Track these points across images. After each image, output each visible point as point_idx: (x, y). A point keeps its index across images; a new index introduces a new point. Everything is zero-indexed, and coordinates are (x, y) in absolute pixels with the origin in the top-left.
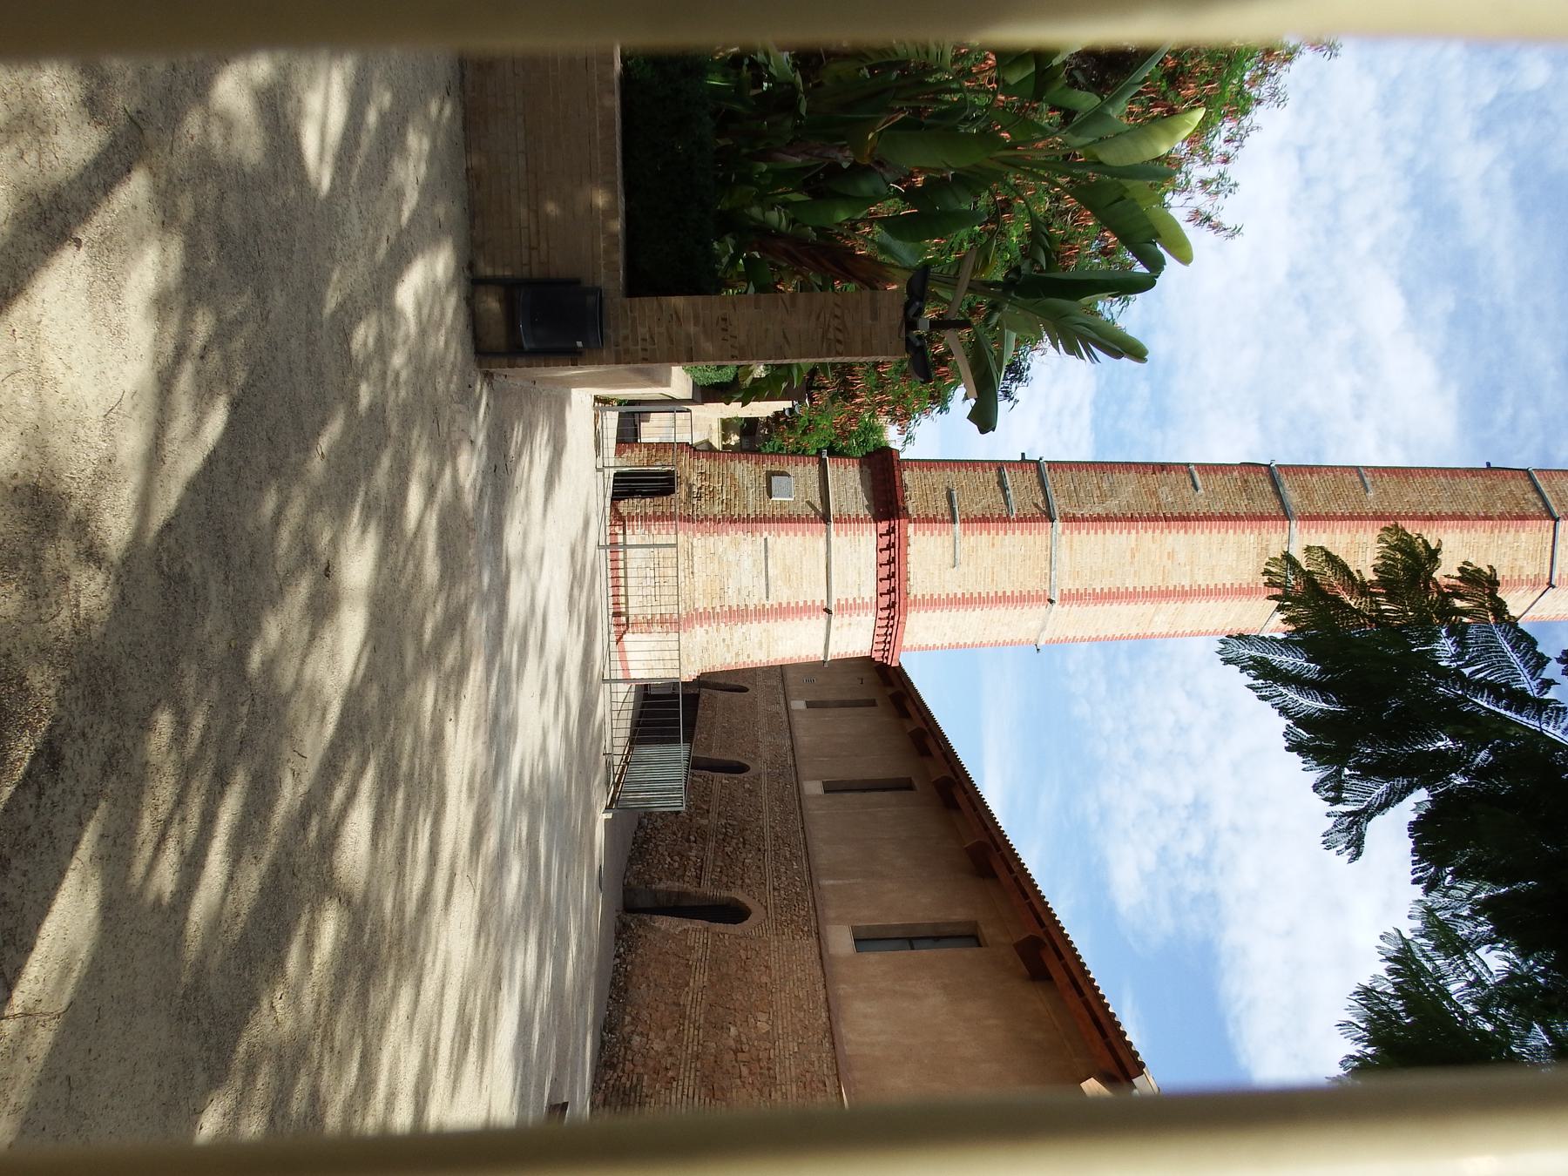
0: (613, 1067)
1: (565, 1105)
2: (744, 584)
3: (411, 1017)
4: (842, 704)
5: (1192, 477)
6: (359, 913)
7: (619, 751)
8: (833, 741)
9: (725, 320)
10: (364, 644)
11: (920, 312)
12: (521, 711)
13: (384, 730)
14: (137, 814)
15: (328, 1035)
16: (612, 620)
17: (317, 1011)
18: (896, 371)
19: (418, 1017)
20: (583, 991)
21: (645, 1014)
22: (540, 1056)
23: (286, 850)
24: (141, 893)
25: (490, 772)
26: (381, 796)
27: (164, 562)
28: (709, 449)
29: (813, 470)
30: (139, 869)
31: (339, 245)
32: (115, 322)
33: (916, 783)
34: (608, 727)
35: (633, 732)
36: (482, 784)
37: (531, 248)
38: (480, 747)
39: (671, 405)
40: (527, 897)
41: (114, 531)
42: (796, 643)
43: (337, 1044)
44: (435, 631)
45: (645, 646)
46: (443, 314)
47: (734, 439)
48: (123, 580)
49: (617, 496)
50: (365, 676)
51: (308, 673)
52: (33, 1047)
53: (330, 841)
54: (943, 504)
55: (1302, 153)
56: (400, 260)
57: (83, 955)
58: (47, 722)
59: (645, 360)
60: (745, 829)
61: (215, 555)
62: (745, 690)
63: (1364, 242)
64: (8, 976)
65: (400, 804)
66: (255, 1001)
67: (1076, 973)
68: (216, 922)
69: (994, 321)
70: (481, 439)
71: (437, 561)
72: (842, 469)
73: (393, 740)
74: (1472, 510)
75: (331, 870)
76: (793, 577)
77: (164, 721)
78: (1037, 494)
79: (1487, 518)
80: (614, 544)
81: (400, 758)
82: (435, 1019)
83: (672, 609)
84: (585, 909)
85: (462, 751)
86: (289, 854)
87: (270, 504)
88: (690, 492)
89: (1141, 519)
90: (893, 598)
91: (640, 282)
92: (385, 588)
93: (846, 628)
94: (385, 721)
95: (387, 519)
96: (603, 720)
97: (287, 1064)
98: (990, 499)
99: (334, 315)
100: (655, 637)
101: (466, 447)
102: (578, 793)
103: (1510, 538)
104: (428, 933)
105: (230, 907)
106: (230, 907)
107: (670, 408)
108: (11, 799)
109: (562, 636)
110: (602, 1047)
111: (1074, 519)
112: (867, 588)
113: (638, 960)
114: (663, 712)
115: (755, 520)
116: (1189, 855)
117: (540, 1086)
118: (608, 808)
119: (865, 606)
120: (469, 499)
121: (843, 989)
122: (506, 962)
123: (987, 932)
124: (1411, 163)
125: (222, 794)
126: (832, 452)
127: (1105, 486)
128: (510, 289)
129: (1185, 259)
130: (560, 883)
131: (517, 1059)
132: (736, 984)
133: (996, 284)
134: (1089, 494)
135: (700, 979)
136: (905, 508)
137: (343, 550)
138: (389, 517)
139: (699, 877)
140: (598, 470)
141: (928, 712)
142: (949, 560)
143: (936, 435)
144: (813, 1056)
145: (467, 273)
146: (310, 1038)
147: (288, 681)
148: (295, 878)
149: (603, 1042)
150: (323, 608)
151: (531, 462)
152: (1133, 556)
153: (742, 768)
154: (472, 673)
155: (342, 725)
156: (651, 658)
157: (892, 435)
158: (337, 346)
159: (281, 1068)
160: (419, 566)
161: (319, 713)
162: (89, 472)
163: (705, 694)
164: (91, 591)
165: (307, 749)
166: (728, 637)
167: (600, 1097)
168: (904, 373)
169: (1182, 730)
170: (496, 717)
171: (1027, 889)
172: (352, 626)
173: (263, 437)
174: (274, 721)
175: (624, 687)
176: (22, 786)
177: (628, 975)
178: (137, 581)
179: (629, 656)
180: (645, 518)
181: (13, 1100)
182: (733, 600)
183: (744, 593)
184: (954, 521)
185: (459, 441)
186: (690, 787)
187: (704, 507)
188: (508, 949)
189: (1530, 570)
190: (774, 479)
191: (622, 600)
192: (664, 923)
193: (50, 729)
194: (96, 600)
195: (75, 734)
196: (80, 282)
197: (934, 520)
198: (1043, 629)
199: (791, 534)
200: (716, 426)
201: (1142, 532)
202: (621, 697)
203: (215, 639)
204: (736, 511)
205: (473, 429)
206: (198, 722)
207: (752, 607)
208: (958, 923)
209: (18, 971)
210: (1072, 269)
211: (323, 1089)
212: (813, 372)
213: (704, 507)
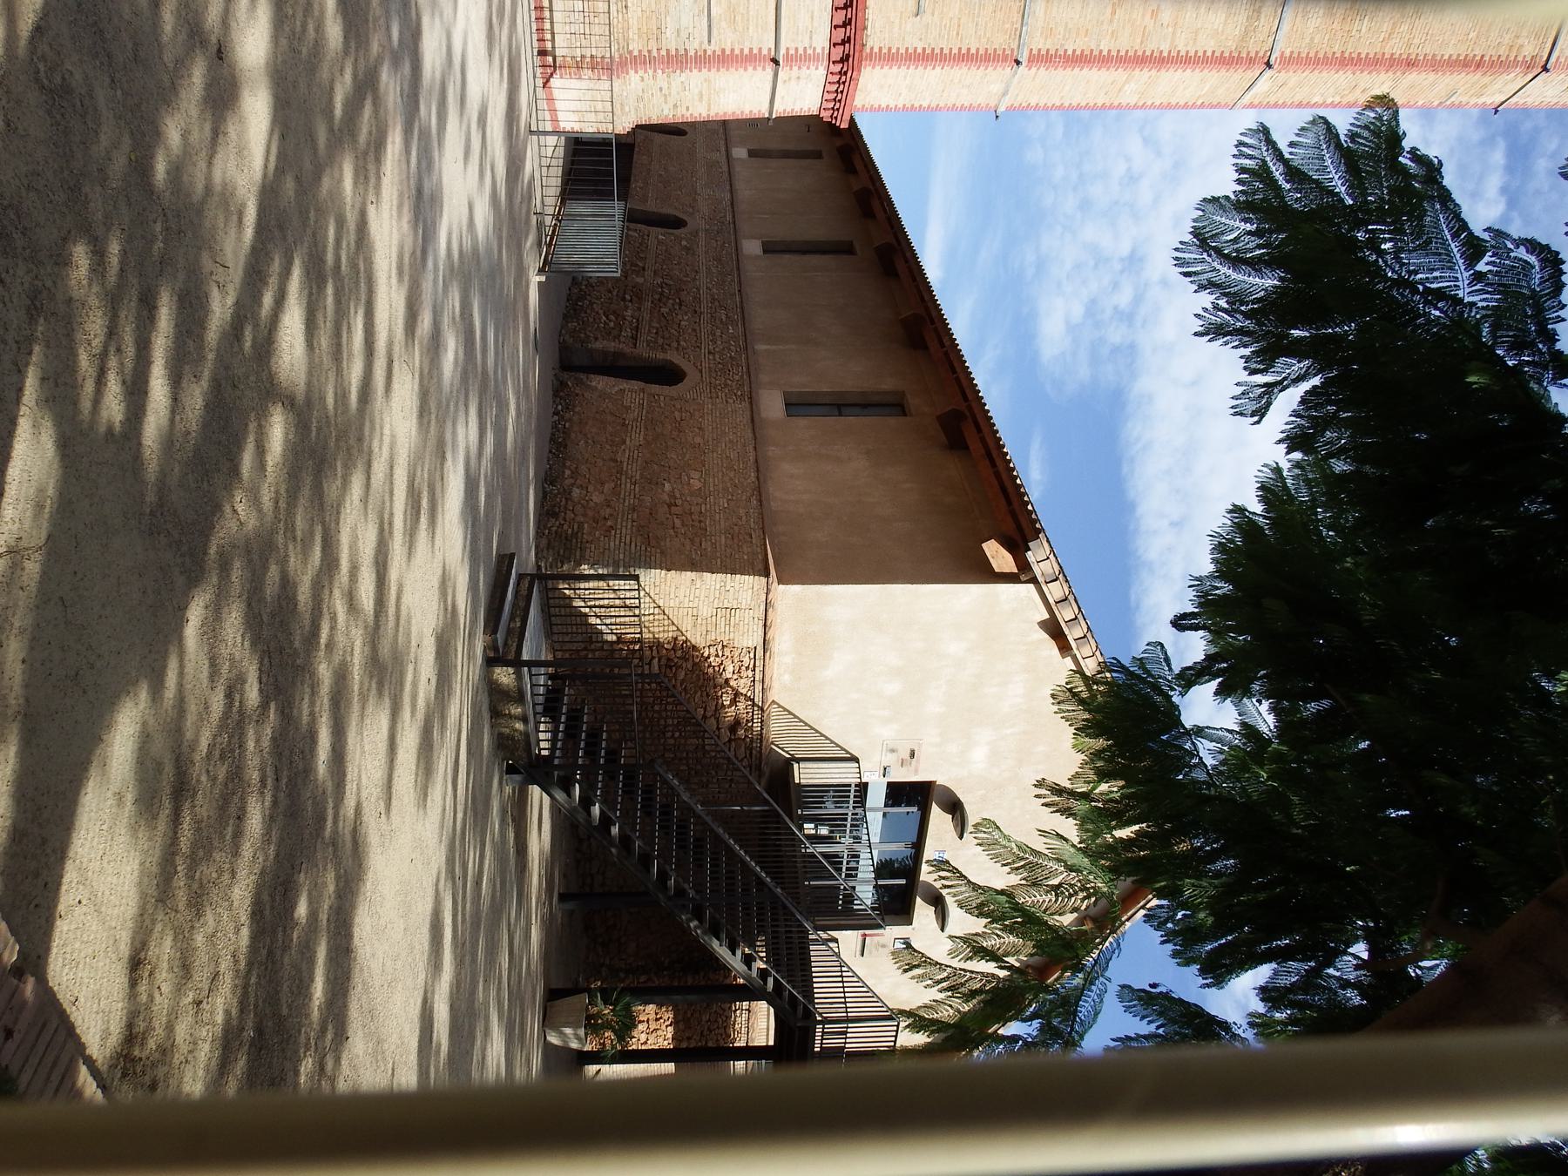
0: (555, 515)
1: (512, 556)
3: (365, 500)
4: (786, 155)
6: (302, 411)
7: (550, 210)
8: (778, 199)
13: (305, 224)
14: (73, 354)
15: (290, 529)
16: (538, 60)
17: (276, 507)
21: (583, 468)
22: (486, 515)
23: (223, 364)
25: (419, 253)
26: (310, 294)
27: (42, 74)
30: (86, 405)
33: (857, 247)
34: (537, 183)
38: (406, 226)
42: (739, 96)
43: (299, 534)
44: (346, 105)
50: (277, 168)
52: (25, 578)
57: (50, 492)
65: (330, 300)
66: (218, 508)
68: (169, 441)
71: (339, 20)
73: (314, 235)
75: (271, 377)
77: (81, 255)
81: (324, 251)
82: (387, 498)
84: (521, 370)
85: (388, 231)
86: (227, 368)
92: (284, 62)
94: (303, 214)
96: (533, 177)
97: (255, 557)
100: (584, 84)
102: (509, 258)
104: (372, 422)
106: (179, 427)
109: (484, 82)
110: (543, 498)
113: (575, 418)
114: (595, 165)
116: (1116, 308)
117: (489, 541)
118: (541, 271)
121: (772, 451)
122: (448, 436)
123: (913, 402)
130: (496, 353)
131: (466, 522)
132: (670, 443)
135: (636, 438)
137: (234, 24)
139: (634, 338)
141: (876, 170)
144: (742, 512)
146: (273, 532)
148: (238, 385)
150: (222, 97)
153: (678, 223)
155: (261, 228)
156: (581, 107)
159: (250, 561)
160: (319, 28)
161: (235, 218)
166: (665, 86)
167: (544, 542)
169: (1132, 179)
170: (419, 191)
172: (256, 111)
174: (190, 234)
175: (552, 140)
177: (566, 432)
178: (19, 102)
179: (559, 105)
181: (17, 624)
182: (671, 43)
183: (684, 35)
186: (625, 241)
188: (449, 424)
189: (1529, 50)
192: (600, 382)
198: (1004, 94)
206: (114, 248)
207: (692, 53)
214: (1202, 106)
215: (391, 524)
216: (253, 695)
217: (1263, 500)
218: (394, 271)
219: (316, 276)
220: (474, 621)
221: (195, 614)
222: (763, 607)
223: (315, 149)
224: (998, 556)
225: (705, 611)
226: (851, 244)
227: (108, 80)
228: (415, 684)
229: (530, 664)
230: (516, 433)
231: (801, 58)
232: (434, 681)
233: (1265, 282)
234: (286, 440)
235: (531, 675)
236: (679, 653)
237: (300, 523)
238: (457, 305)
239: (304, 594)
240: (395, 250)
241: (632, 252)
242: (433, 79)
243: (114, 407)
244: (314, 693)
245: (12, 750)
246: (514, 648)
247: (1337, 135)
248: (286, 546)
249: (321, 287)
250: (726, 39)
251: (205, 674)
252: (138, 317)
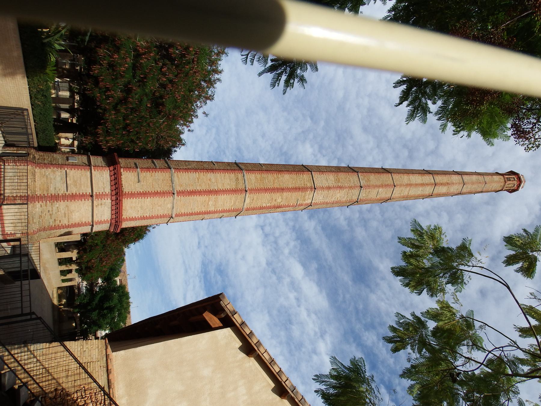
45: (12, 211)
55: (262, 228)
63: (286, 251)
76: (78, 184)
90: (117, 193)
93: (100, 206)
103: (301, 176)
119: (107, 195)
124: (294, 227)
142: (136, 179)
166: (51, 210)
179: (6, 225)
182: (52, 191)
184: (137, 168)
199: (76, 169)
222: (105, 359)
231: (101, 196)
250: (73, 190)
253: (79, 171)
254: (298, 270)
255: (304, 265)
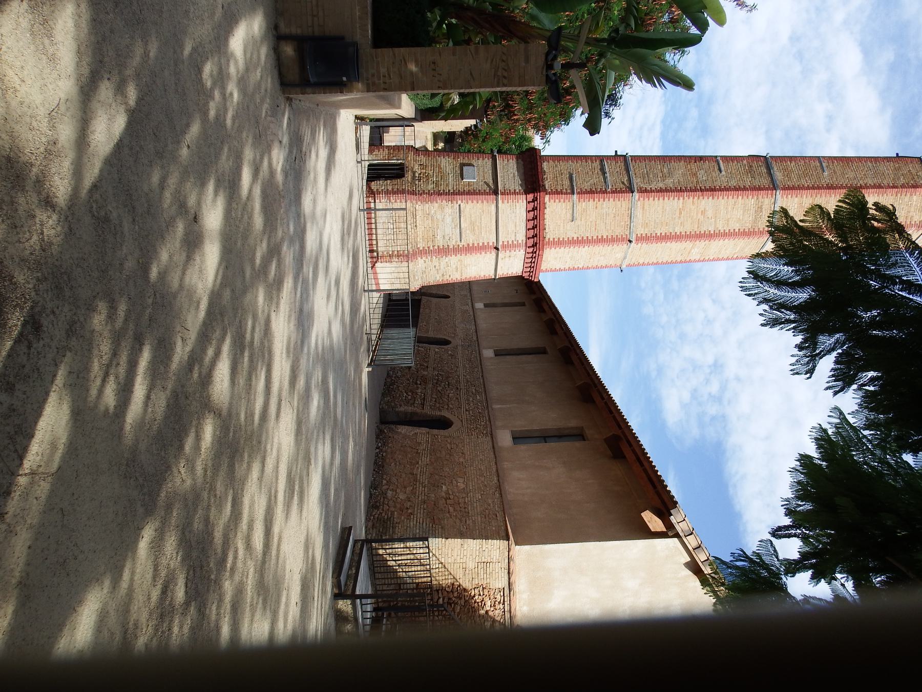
0: (377, 508)
1: (351, 527)
2: (447, 233)
3: (260, 479)
5: (719, 164)
6: (226, 421)
7: (374, 332)
8: (499, 326)
9: (434, 63)
10: (220, 264)
11: (555, 58)
12: (316, 308)
14: (89, 359)
15: (212, 489)
16: (369, 255)
17: (205, 471)
18: (539, 99)
19: (264, 479)
20: (358, 467)
21: (394, 480)
22: (335, 501)
24: (96, 406)
25: (299, 342)
26: (235, 354)
27: (94, 209)
28: (424, 150)
29: (488, 162)
30: (94, 392)
31: (192, 10)
32: (51, 51)
33: (548, 350)
34: (368, 318)
35: (383, 321)
36: (295, 349)
37: (313, 16)
39: (402, 122)
40: (324, 414)
41: (61, 188)
42: (478, 268)
43: (218, 493)
44: (263, 258)
45: (388, 270)
46: (259, 58)
47: (441, 145)
48: (70, 218)
49: (370, 179)
50: (222, 283)
51: (187, 279)
52: (39, 492)
53: (207, 379)
54: (567, 183)
56: (229, 22)
57: (64, 440)
58: (29, 304)
59: (385, 90)
60: (448, 377)
61: (126, 206)
62: (448, 297)
63: (839, 16)
64: (20, 452)
65: (246, 359)
66: (169, 468)
67: (639, 454)
68: (141, 424)
69: (600, 65)
70: (285, 140)
72: (506, 162)
73: (240, 322)
74: (885, 182)
75: (208, 397)
76: (476, 228)
78: (625, 176)
79: (894, 187)
80: (369, 209)
83: (403, 248)
84: (360, 422)
85: (282, 328)
86: (183, 386)
87: (155, 178)
88: (414, 177)
89: (686, 190)
90: (536, 241)
91: (382, 39)
93: (507, 259)
95: (230, 188)
96: (364, 320)
97: (190, 503)
98: (596, 180)
99: (191, 54)
100: (394, 264)
101: (276, 144)
105: (149, 416)
107: (401, 123)
108: (12, 348)
109: (339, 263)
111: (646, 191)
112: (521, 235)
113: (389, 450)
114: (401, 309)
115: (454, 193)
117: (336, 518)
118: (369, 365)
120: (279, 177)
121: (506, 465)
122: (312, 449)
123: (588, 432)
125: (141, 350)
126: (499, 152)
127: (665, 170)
128: (300, 41)
129: (721, 22)
130: (343, 407)
133: (603, 40)
134: (655, 175)
135: (425, 460)
136: (544, 186)
137: (204, 206)
138: (231, 186)
140: (358, 162)
141: (556, 309)
142: (569, 216)
143: (565, 140)
145: (274, 33)
147: (175, 284)
148: (186, 401)
149: (371, 494)
150: (193, 242)
151: (317, 156)
152: (680, 213)
153: (447, 342)
154: (285, 285)
155: (209, 312)
156: (391, 277)
157: (537, 142)
158: (193, 76)
160: (251, 217)
162: (42, 149)
163: (424, 299)
164: (49, 226)
165: (189, 325)
166: (437, 264)
167: (370, 524)
168: (545, 100)
170: (301, 310)
171: (612, 408)
173: (148, 135)
176: (17, 341)
177: (383, 459)
178: (79, 220)
179: (380, 276)
180: (387, 193)
181: (29, 521)
182: (440, 242)
183: (447, 238)
184: (573, 193)
185: (272, 141)
186: (417, 353)
187: (422, 186)
190: (465, 168)
191: (374, 242)
192: (403, 430)
193: (32, 308)
194: (53, 231)
195: (48, 311)
196: (24, 23)
197: (561, 193)
198: (625, 258)
200: (430, 137)
201: (686, 198)
202: (375, 301)
203: (129, 257)
204: (442, 188)
205: (280, 134)
206: (122, 308)
207: (451, 247)
208: (572, 428)
209: (26, 449)
210: (651, 33)
211: (212, 518)
212: (489, 101)
213: (422, 186)
214: (737, 258)
215: (276, 497)
216: (180, 593)
217: (819, 446)
218: (284, 352)
219: (239, 345)
220: (326, 569)
221: (148, 534)
222: (507, 561)
223: (244, 277)
224: (654, 522)
225: (471, 565)
226: (545, 348)
227: (131, 220)
228: (287, 605)
229: (361, 597)
230: (354, 454)
232: (299, 605)
233: (802, 296)
234: (214, 435)
235: (362, 605)
236: (456, 594)
237: (220, 487)
238: (320, 375)
239: (218, 535)
240: (285, 338)
241: (422, 359)
242: (311, 255)
243: (110, 397)
244: (221, 600)
245: (10, 609)
246: (351, 587)
247: (829, 214)
248: (209, 498)
249: (242, 352)
250: (470, 239)
251: (149, 576)
252: (133, 348)
253: (479, 205)
254: (849, 59)
255: (867, 52)
